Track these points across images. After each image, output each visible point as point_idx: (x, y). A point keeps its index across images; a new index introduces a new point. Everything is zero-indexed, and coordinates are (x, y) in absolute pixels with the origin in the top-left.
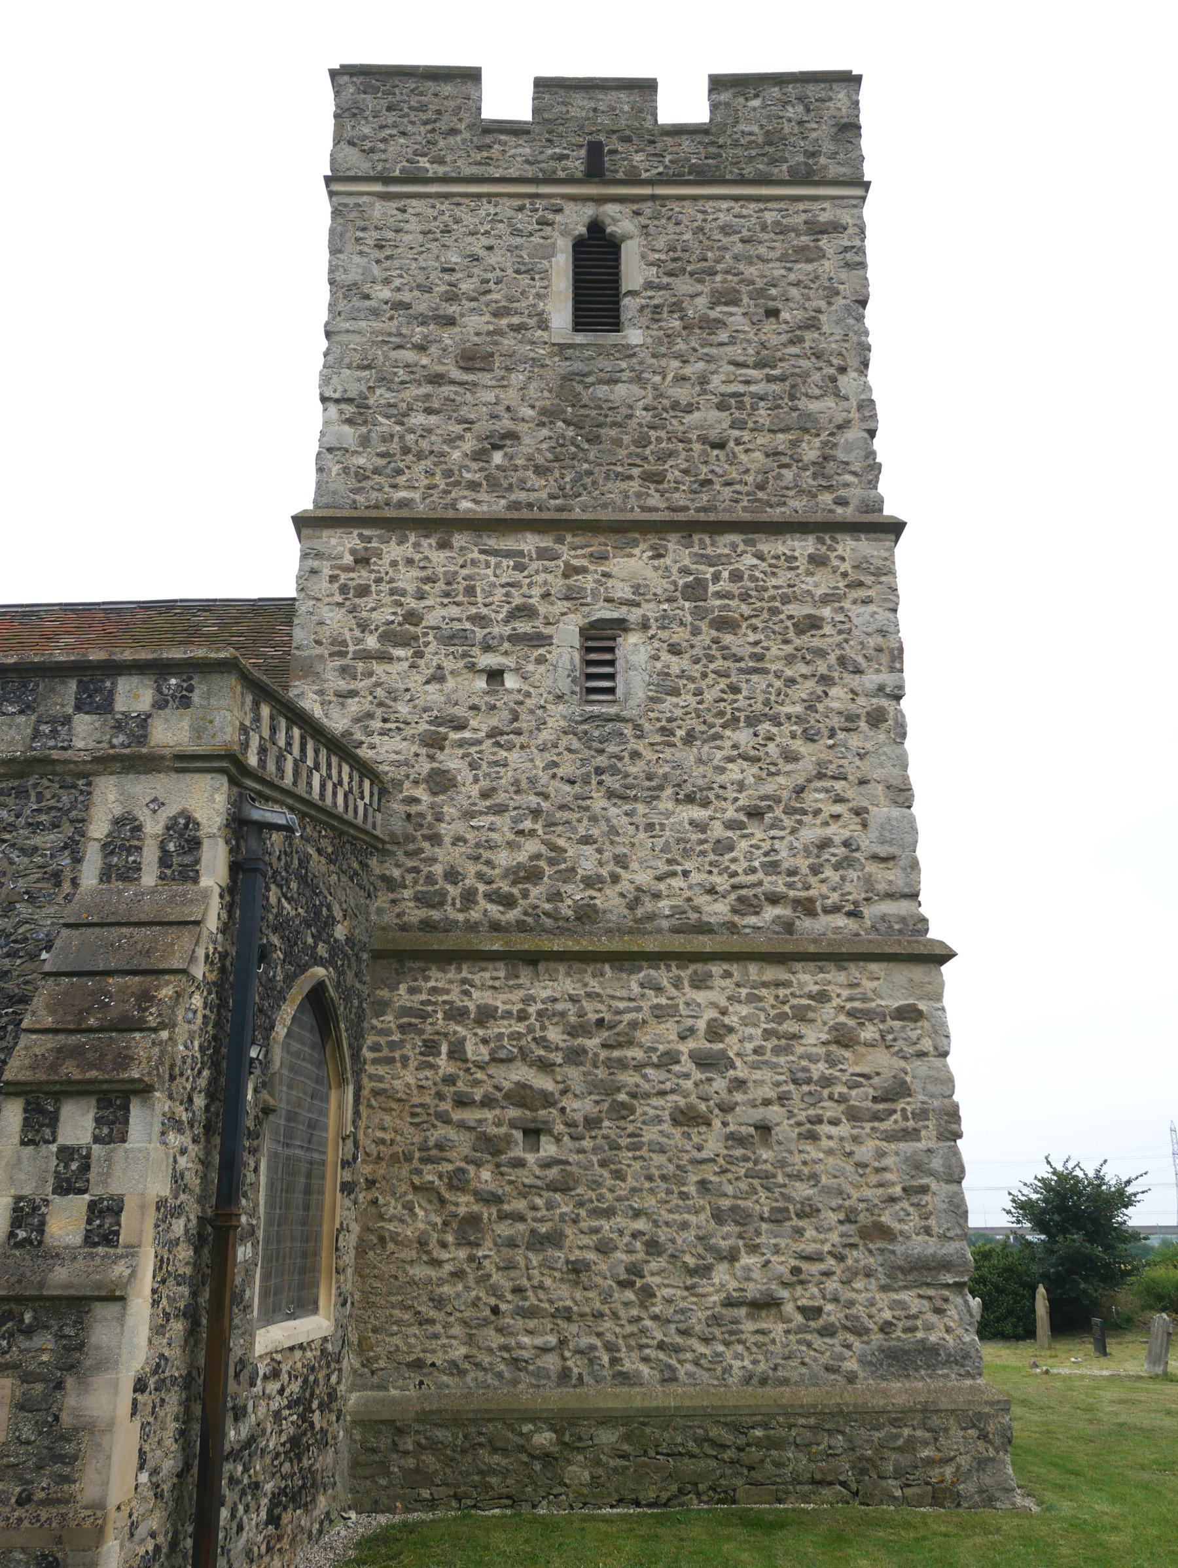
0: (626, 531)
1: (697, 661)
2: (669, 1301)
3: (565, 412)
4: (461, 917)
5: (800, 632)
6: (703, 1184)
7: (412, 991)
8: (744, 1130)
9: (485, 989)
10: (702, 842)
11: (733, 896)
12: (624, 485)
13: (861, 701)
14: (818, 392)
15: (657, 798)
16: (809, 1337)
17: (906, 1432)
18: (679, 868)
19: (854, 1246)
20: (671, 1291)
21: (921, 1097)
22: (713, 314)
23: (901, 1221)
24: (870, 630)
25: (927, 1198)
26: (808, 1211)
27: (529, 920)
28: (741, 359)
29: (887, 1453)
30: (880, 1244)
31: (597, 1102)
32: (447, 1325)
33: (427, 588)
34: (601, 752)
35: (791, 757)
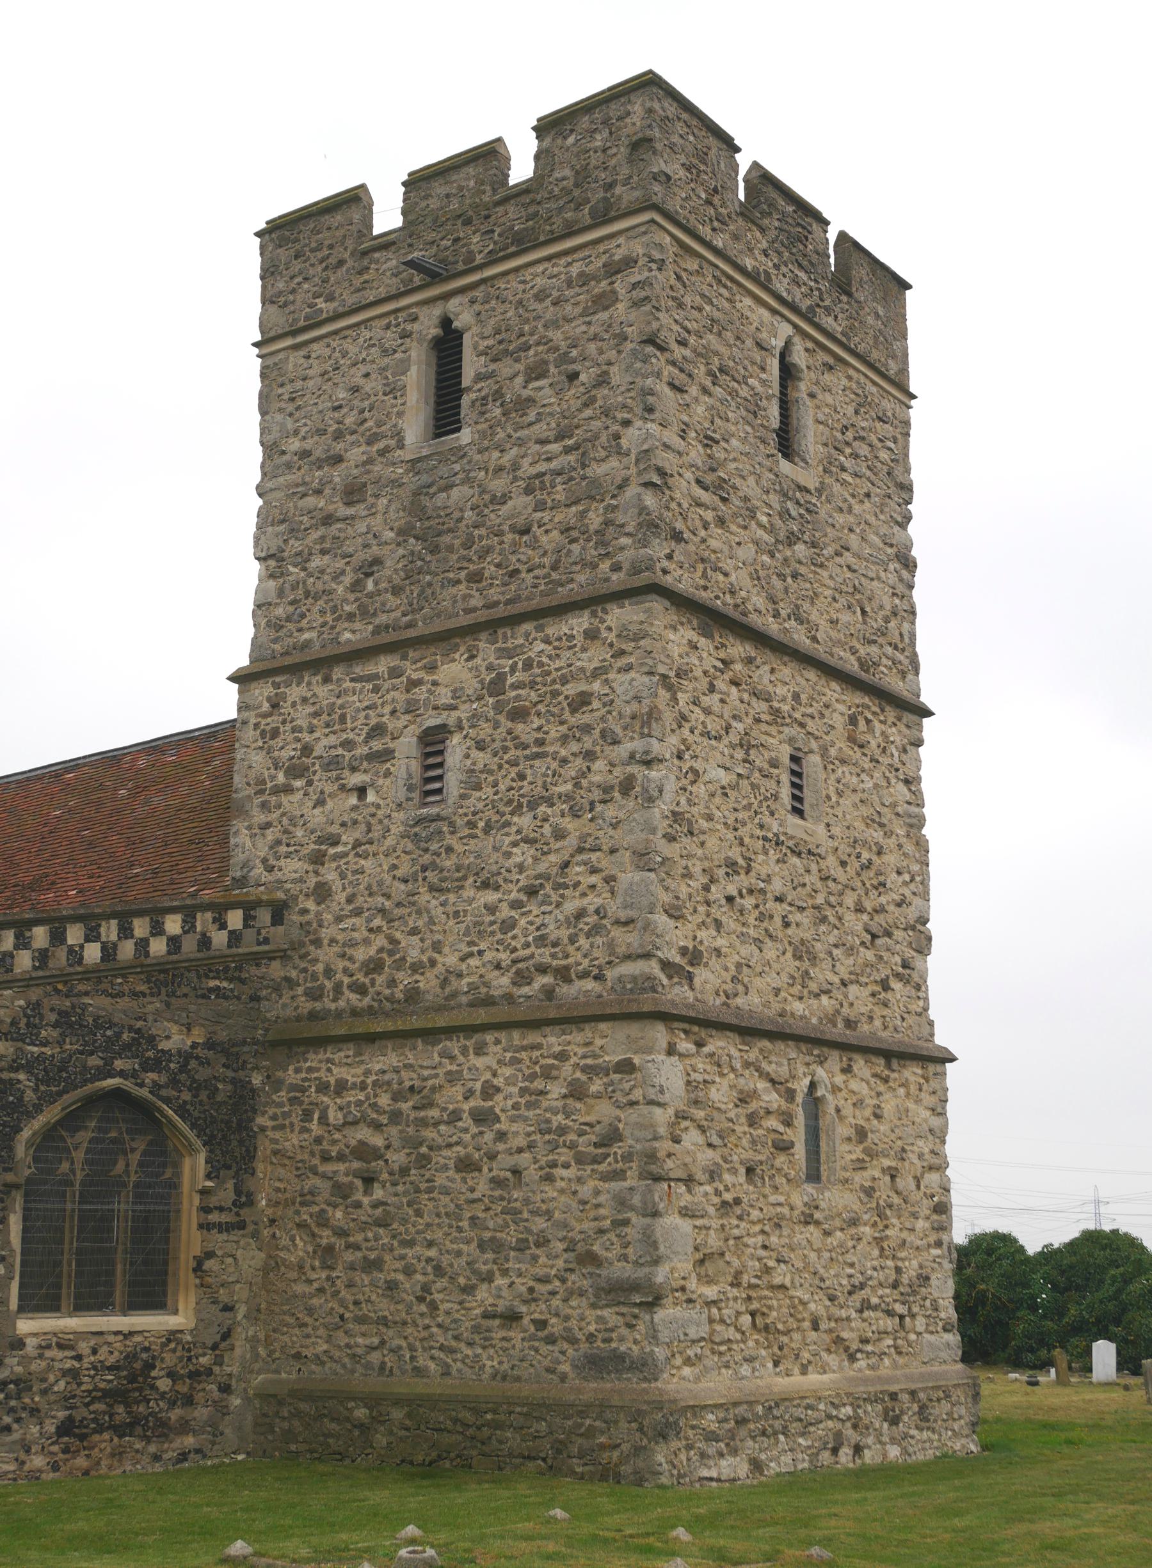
0: (445, 639)
1: (495, 755)
2: (448, 1313)
3: (414, 528)
4: (333, 1006)
5: (574, 711)
6: (473, 1219)
7: (298, 1071)
8: (502, 1174)
9: (340, 1066)
10: (492, 923)
11: (514, 970)
12: (453, 591)
13: (617, 771)
14: (603, 454)
15: (461, 887)
16: (536, 1344)
17: (588, 1422)
18: (476, 949)
19: (572, 1270)
20: (449, 1305)
21: (630, 1142)
22: (526, 393)
23: (607, 1249)
24: (628, 698)
25: (628, 1230)
26: (542, 1242)
27: (375, 1004)
28: (544, 436)
29: (574, 1438)
30: (590, 1269)
31: (408, 1155)
32: (315, 1328)
33: (315, 721)
34: (426, 850)
35: (560, 834)
